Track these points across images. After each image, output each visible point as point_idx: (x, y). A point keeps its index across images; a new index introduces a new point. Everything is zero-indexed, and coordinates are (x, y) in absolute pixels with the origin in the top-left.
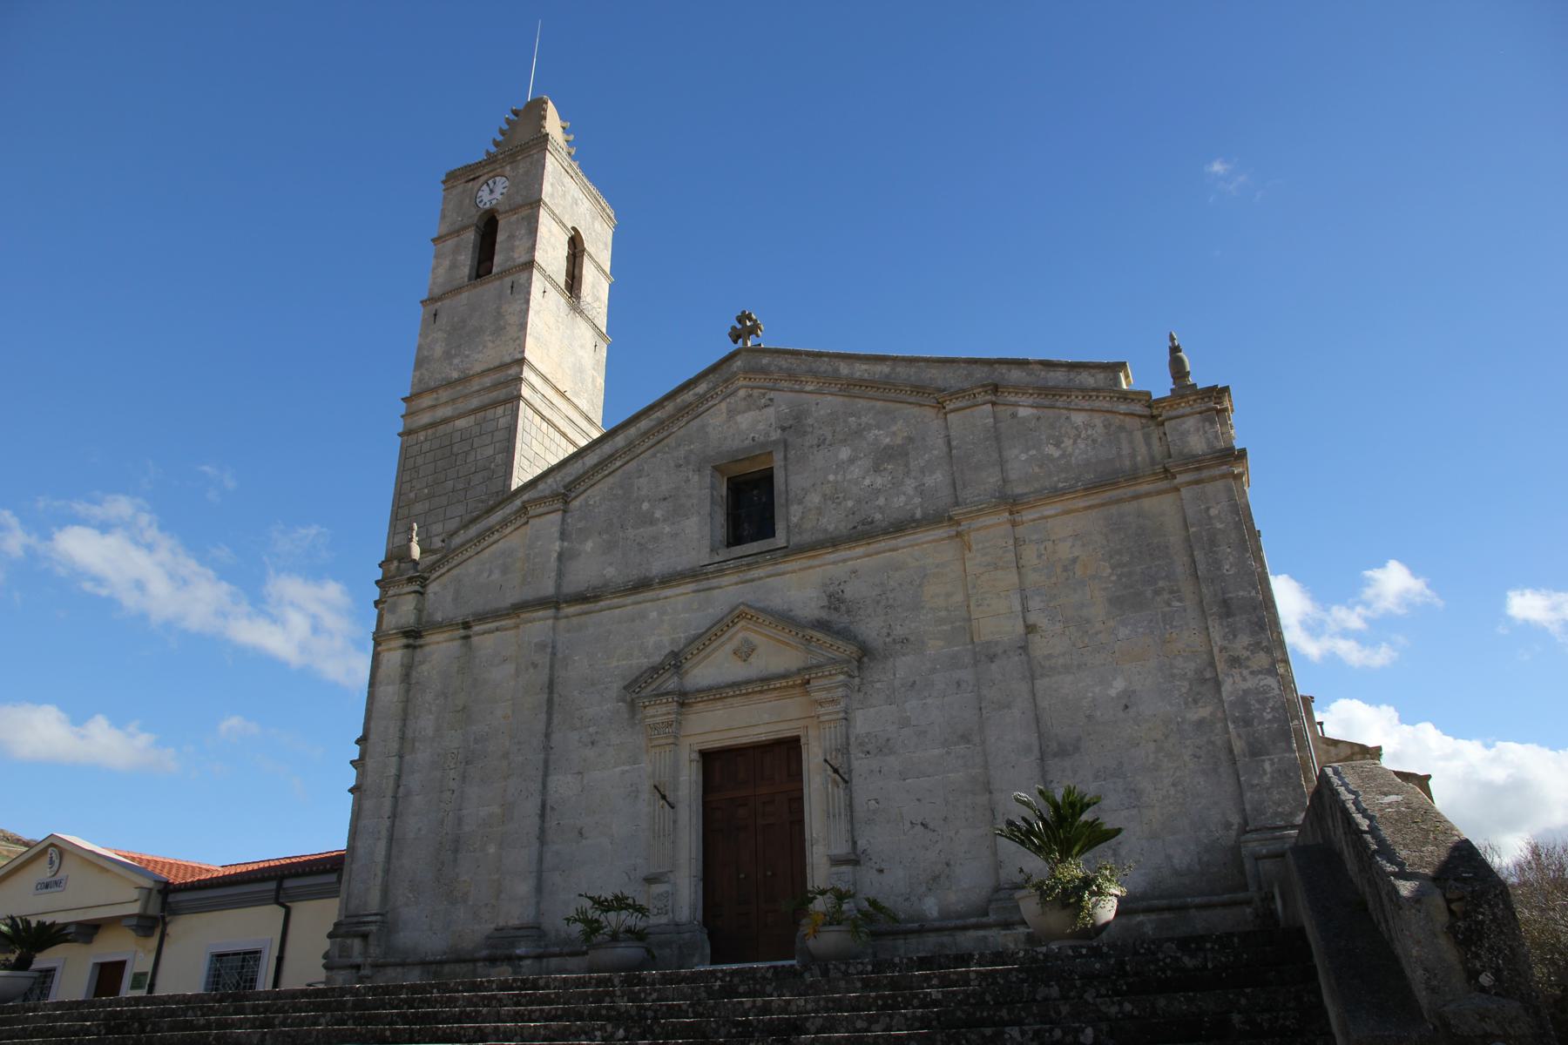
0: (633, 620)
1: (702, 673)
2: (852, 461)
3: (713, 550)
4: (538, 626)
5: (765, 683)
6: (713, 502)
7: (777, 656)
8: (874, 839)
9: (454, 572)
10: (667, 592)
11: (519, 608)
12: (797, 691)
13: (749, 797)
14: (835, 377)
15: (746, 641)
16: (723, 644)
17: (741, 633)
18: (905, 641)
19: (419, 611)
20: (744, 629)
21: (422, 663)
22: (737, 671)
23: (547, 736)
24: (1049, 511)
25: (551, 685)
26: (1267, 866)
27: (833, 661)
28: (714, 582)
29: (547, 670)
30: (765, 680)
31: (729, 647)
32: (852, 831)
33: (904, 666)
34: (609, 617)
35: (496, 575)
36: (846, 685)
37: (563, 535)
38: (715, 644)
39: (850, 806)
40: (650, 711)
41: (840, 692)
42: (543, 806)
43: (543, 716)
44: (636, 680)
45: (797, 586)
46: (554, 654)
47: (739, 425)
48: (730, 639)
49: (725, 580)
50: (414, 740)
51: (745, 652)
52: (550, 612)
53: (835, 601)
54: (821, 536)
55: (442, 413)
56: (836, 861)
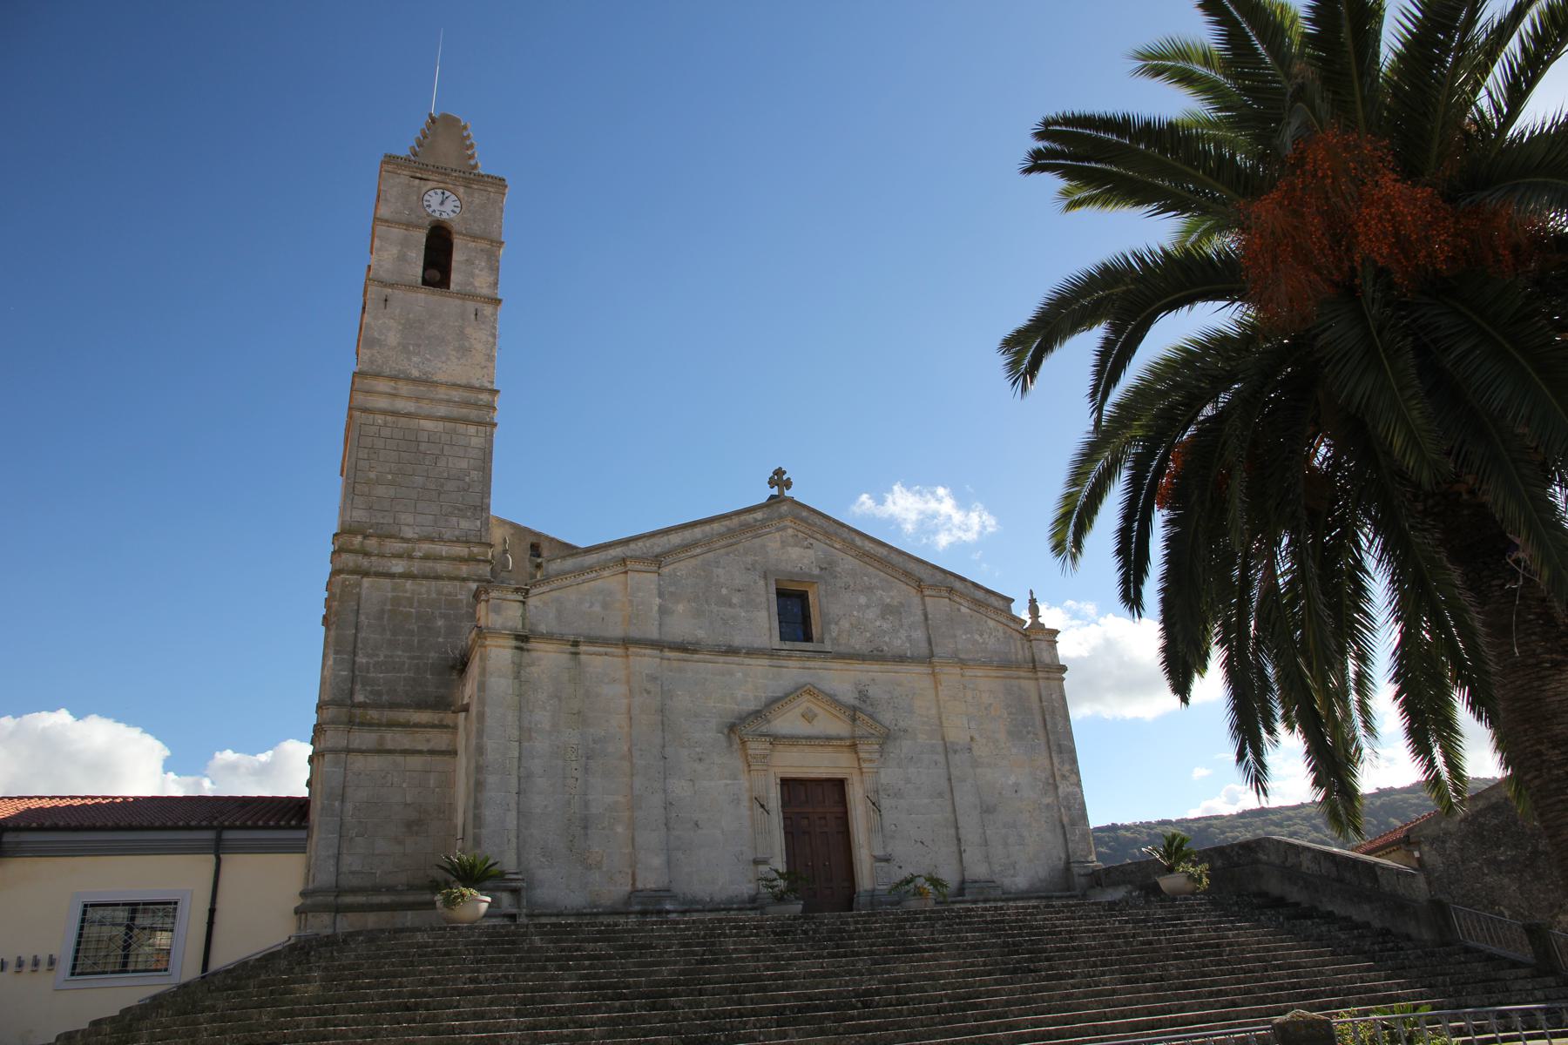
1: (787, 722)
2: (868, 606)
4: (646, 661)
5: (826, 740)
7: (835, 726)
9: (554, 594)
11: (627, 642)
13: (815, 811)
14: (853, 545)
17: (805, 703)
18: (905, 731)
19: (524, 617)
21: (532, 664)
24: (979, 673)
26: (1083, 880)
30: (829, 738)
34: (703, 667)
35: (597, 608)
47: (797, 557)
49: (790, 663)
50: (530, 730)
51: (809, 717)
52: (656, 652)
53: (863, 696)
55: (400, 405)
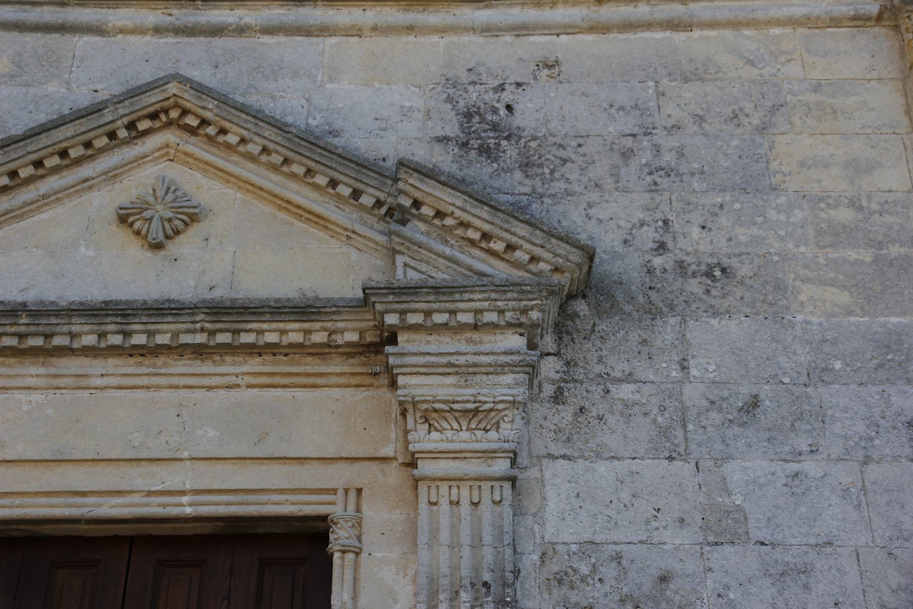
18: (717, 273)
20: (167, 154)
31: (105, 201)
33: (716, 347)
38: (53, 183)
51: (160, 225)
53: (483, 129)
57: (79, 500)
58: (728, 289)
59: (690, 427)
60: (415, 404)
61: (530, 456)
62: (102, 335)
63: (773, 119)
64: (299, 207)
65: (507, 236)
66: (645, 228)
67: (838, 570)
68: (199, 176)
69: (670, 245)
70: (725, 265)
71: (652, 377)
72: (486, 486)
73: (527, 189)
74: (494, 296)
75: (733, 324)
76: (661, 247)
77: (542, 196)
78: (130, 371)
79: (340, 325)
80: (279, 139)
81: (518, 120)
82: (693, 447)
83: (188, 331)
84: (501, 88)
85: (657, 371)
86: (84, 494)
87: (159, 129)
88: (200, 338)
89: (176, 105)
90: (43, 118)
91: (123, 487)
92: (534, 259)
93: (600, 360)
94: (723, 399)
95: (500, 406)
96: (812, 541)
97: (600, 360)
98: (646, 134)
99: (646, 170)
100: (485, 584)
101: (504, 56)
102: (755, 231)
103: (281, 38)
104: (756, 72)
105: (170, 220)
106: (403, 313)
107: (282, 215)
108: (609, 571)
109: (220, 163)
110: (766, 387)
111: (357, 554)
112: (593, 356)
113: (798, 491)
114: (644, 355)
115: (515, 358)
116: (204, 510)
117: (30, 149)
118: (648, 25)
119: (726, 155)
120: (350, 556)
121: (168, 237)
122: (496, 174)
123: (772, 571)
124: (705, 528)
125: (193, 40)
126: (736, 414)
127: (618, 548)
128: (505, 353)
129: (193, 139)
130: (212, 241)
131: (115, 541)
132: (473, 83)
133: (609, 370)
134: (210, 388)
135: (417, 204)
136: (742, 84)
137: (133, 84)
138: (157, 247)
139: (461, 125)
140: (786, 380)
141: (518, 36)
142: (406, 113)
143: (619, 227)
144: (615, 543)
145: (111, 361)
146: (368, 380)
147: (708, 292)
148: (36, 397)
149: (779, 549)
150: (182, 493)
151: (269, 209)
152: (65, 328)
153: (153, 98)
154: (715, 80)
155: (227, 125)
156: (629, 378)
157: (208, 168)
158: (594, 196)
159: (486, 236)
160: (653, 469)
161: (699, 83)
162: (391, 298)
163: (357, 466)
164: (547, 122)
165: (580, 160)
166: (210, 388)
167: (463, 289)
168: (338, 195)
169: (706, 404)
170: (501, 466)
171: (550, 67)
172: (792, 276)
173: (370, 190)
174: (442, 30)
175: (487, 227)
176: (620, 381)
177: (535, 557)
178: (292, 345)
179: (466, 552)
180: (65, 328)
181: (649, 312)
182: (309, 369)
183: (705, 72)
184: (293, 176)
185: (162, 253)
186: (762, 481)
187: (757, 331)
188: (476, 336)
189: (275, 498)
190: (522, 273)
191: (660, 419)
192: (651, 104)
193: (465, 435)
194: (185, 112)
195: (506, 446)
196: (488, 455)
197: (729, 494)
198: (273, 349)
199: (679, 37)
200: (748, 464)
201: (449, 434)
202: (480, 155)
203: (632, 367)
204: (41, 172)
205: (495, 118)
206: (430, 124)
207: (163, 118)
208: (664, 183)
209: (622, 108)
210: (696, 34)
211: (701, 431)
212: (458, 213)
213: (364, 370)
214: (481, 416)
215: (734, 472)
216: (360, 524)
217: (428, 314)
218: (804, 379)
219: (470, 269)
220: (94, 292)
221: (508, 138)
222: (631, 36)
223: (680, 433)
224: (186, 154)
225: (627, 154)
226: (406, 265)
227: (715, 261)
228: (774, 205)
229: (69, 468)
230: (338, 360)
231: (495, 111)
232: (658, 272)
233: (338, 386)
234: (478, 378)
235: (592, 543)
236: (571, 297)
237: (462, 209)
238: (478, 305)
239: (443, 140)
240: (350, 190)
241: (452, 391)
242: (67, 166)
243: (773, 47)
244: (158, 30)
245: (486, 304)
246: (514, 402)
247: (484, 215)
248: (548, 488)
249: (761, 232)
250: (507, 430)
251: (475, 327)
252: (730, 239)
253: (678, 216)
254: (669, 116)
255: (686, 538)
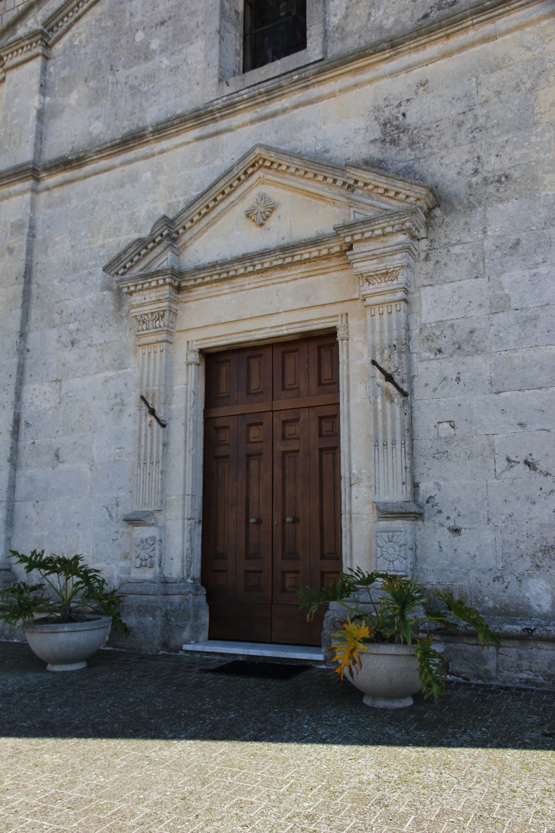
0: (122, 186)
1: (204, 247)
3: (222, 80)
5: (287, 256)
6: (223, 14)
7: (304, 215)
8: (446, 482)
10: (165, 144)
12: (335, 262)
15: (263, 197)
16: (233, 204)
18: (503, 179)
20: (261, 181)
22: (252, 239)
23: (23, 335)
25: (28, 274)
27: (391, 215)
28: (223, 124)
29: (23, 256)
31: (241, 209)
32: (412, 468)
33: (500, 218)
34: (95, 185)
36: (408, 249)
37: (44, 89)
38: (222, 206)
39: (410, 431)
40: (137, 298)
41: (398, 259)
42: (17, 422)
43: (18, 312)
44: (118, 258)
45: (335, 115)
46: (32, 236)
48: (242, 197)
51: (261, 215)
52: (28, 184)
53: (392, 130)
54: (374, 38)
56: (387, 513)
57: (249, 334)
58: (508, 186)
59: (486, 261)
60: (361, 275)
61: (415, 287)
62: (246, 268)
63: (538, 82)
64: (313, 193)
65: (394, 188)
66: (468, 163)
67: (551, 316)
68: (273, 188)
69: (480, 170)
70: (507, 174)
71: (469, 240)
72: (393, 305)
73: (413, 157)
74: (388, 220)
75: (509, 205)
76: (476, 172)
77: (419, 159)
78: (257, 280)
79: (331, 245)
80: (301, 163)
81: (408, 120)
82: (487, 270)
83: (275, 260)
84: (400, 105)
85: (472, 237)
86: (250, 331)
87: (257, 170)
88: (280, 262)
89: (261, 158)
90: (215, 177)
91: (262, 327)
92: (407, 197)
93: (446, 236)
94: (502, 244)
95: (396, 269)
96: (540, 304)
97: (446, 236)
98: (470, 110)
99: (470, 131)
100: (394, 345)
101: (399, 86)
102: (524, 151)
103: (301, 109)
104: (531, 54)
105: (264, 212)
106: (352, 236)
107: (307, 198)
108: (448, 332)
109: (280, 180)
110: (524, 234)
111: (348, 340)
112: (442, 235)
113: (535, 282)
114: (466, 230)
115: (401, 246)
116: (291, 331)
117: (210, 194)
118: (473, 44)
119: (511, 110)
120: (345, 341)
121: (265, 220)
122: (398, 153)
123: (520, 321)
124: (491, 307)
125: (266, 122)
126: (508, 250)
127: (452, 322)
128: (396, 245)
129: (270, 172)
130: (282, 217)
131: (266, 346)
132: (387, 106)
133: (450, 241)
134: (287, 282)
135: (356, 182)
136: (523, 64)
137: (246, 151)
138: (261, 225)
139: (382, 131)
140: (534, 228)
141: (407, 72)
142: (356, 132)
143: (456, 166)
144: (451, 320)
145: (252, 277)
146: (346, 266)
147: (498, 190)
148: (229, 297)
149: (524, 310)
150: (283, 325)
151: (301, 197)
152: (232, 268)
153: (251, 158)
154: (508, 66)
155: (281, 162)
156: (459, 242)
157: (277, 184)
158: (444, 153)
159: (386, 190)
160: (469, 284)
161: (499, 71)
162: (346, 230)
163: (345, 304)
164: (421, 118)
165: (437, 134)
166: (287, 282)
167: (374, 220)
168: (328, 183)
169: (494, 248)
170: (400, 295)
171: (423, 85)
172: (541, 172)
173: (340, 178)
174: (371, 81)
175: (385, 186)
176: (455, 245)
177: (417, 331)
178: (315, 257)
179: (386, 334)
180: (232, 268)
181: (469, 207)
182: (322, 266)
183: (503, 63)
184: (309, 179)
185: (264, 227)
186: (519, 280)
187: (521, 206)
188: (384, 239)
189: (315, 322)
190: (404, 204)
191: (472, 260)
192: (474, 92)
193: (383, 284)
194: (265, 160)
195: (400, 286)
196: (394, 291)
197: (503, 289)
198: (308, 260)
199: (489, 46)
200: (512, 274)
201: (377, 285)
202: (391, 144)
203: (460, 236)
204: (217, 203)
205: (397, 122)
206: (368, 134)
207: (257, 165)
208: (478, 135)
209: (459, 99)
210: (500, 40)
211: (491, 262)
212: (373, 182)
213: (345, 262)
214: (389, 275)
215: (506, 279)
216: (348, 328)
217: (363, 234)
218: (543, 225)
219: (380, 208)
220: (239, 250)
221: (403, 132)
222: (464, 53)
223: (481, 265)
224: (268, 180)
225: (460, 125)
226: (354, 212)
227: (502, 173)
228: (534, 133)
229: (243, 322)
230: (334, 259)
231: (397, 118)
232: (474, 186)
233: (335, 271)
234: (386, 258)
235: (441, 321)
236: (430, 210)
237: (374, 180)
238: (382, 225)
239: (374, 141)
240: (332, 180)
241: (376, 266)
242: (226, 197)
243: (542, 34)
244: (252, 122)
245: (386, 224)
246: (402, 266)
247: (384, 181)
248: (423, 300)
249: (527, 151)
250: (401, 279)
251: (384, 235)
252: (510, 159)
253: (485, 153)
254: (483, 96)
255: (482, 313)
